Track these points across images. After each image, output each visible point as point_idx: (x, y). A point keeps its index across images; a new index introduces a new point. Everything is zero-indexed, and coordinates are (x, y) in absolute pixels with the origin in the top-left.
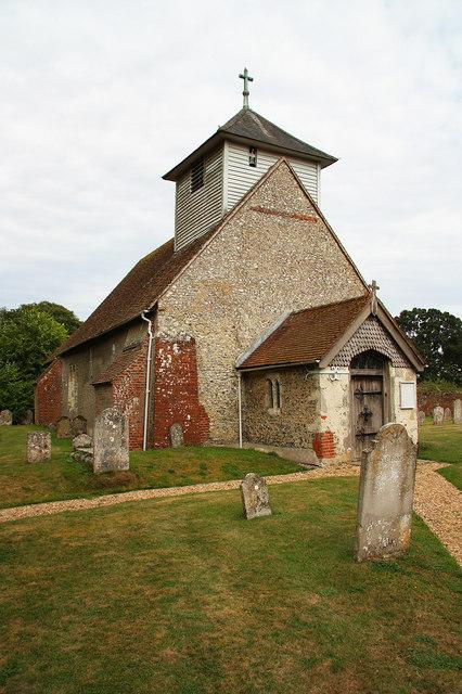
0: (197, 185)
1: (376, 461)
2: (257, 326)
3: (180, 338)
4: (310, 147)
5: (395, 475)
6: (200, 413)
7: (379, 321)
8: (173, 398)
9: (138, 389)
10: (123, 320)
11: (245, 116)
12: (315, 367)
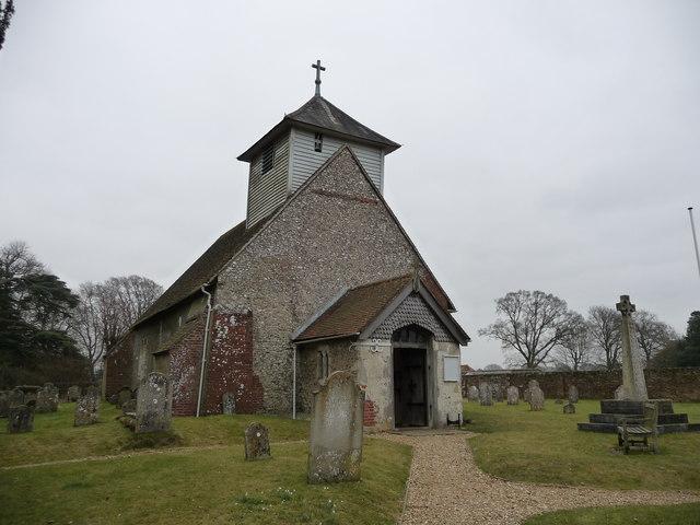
0: (267, 168)
2: (315, 302)
3: (238, 311)
5: (343, 414)
6: (255, 383)
7: (421, 297)
9: (195, 359)
10: (183, 296)
11: (317, 103)
12: (355, 338)
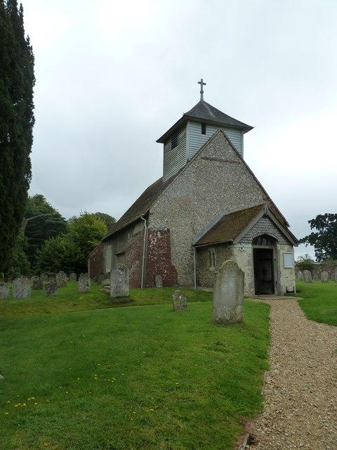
0: (174, 146)
1: (221, 278)
2: (203, 224)
4: (238, 121)
6: (172, 269)
7: (270, 218)
8: (157, 261)
9: (139, 256)
11: (202, 106)
12: (230, 243)
